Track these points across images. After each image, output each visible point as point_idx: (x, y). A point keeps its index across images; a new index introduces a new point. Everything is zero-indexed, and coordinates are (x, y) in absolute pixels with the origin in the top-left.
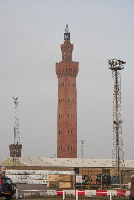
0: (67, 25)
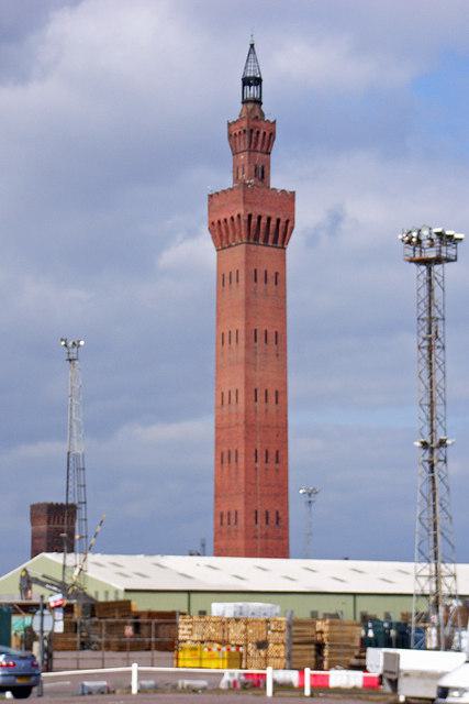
0: (252, 46)
